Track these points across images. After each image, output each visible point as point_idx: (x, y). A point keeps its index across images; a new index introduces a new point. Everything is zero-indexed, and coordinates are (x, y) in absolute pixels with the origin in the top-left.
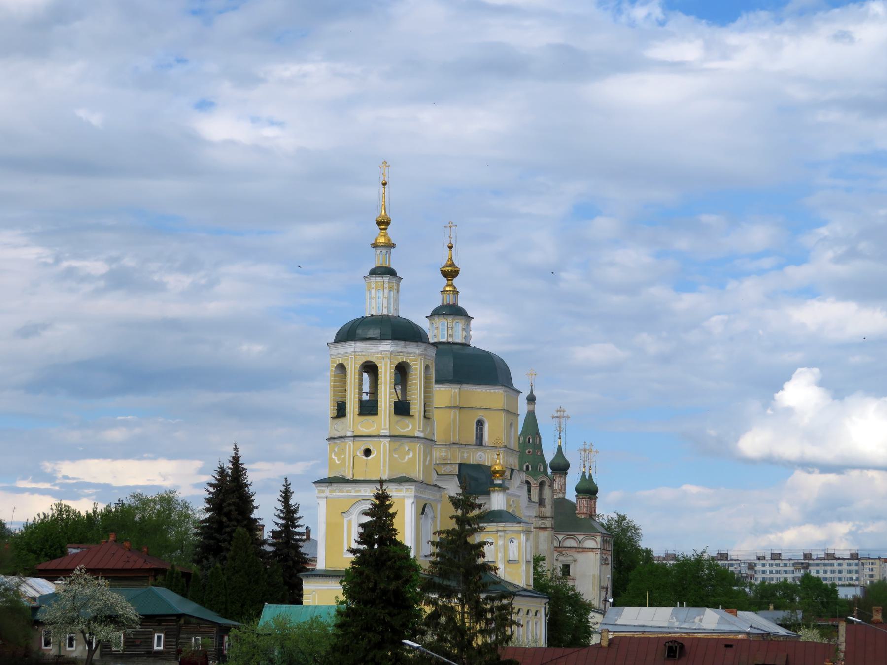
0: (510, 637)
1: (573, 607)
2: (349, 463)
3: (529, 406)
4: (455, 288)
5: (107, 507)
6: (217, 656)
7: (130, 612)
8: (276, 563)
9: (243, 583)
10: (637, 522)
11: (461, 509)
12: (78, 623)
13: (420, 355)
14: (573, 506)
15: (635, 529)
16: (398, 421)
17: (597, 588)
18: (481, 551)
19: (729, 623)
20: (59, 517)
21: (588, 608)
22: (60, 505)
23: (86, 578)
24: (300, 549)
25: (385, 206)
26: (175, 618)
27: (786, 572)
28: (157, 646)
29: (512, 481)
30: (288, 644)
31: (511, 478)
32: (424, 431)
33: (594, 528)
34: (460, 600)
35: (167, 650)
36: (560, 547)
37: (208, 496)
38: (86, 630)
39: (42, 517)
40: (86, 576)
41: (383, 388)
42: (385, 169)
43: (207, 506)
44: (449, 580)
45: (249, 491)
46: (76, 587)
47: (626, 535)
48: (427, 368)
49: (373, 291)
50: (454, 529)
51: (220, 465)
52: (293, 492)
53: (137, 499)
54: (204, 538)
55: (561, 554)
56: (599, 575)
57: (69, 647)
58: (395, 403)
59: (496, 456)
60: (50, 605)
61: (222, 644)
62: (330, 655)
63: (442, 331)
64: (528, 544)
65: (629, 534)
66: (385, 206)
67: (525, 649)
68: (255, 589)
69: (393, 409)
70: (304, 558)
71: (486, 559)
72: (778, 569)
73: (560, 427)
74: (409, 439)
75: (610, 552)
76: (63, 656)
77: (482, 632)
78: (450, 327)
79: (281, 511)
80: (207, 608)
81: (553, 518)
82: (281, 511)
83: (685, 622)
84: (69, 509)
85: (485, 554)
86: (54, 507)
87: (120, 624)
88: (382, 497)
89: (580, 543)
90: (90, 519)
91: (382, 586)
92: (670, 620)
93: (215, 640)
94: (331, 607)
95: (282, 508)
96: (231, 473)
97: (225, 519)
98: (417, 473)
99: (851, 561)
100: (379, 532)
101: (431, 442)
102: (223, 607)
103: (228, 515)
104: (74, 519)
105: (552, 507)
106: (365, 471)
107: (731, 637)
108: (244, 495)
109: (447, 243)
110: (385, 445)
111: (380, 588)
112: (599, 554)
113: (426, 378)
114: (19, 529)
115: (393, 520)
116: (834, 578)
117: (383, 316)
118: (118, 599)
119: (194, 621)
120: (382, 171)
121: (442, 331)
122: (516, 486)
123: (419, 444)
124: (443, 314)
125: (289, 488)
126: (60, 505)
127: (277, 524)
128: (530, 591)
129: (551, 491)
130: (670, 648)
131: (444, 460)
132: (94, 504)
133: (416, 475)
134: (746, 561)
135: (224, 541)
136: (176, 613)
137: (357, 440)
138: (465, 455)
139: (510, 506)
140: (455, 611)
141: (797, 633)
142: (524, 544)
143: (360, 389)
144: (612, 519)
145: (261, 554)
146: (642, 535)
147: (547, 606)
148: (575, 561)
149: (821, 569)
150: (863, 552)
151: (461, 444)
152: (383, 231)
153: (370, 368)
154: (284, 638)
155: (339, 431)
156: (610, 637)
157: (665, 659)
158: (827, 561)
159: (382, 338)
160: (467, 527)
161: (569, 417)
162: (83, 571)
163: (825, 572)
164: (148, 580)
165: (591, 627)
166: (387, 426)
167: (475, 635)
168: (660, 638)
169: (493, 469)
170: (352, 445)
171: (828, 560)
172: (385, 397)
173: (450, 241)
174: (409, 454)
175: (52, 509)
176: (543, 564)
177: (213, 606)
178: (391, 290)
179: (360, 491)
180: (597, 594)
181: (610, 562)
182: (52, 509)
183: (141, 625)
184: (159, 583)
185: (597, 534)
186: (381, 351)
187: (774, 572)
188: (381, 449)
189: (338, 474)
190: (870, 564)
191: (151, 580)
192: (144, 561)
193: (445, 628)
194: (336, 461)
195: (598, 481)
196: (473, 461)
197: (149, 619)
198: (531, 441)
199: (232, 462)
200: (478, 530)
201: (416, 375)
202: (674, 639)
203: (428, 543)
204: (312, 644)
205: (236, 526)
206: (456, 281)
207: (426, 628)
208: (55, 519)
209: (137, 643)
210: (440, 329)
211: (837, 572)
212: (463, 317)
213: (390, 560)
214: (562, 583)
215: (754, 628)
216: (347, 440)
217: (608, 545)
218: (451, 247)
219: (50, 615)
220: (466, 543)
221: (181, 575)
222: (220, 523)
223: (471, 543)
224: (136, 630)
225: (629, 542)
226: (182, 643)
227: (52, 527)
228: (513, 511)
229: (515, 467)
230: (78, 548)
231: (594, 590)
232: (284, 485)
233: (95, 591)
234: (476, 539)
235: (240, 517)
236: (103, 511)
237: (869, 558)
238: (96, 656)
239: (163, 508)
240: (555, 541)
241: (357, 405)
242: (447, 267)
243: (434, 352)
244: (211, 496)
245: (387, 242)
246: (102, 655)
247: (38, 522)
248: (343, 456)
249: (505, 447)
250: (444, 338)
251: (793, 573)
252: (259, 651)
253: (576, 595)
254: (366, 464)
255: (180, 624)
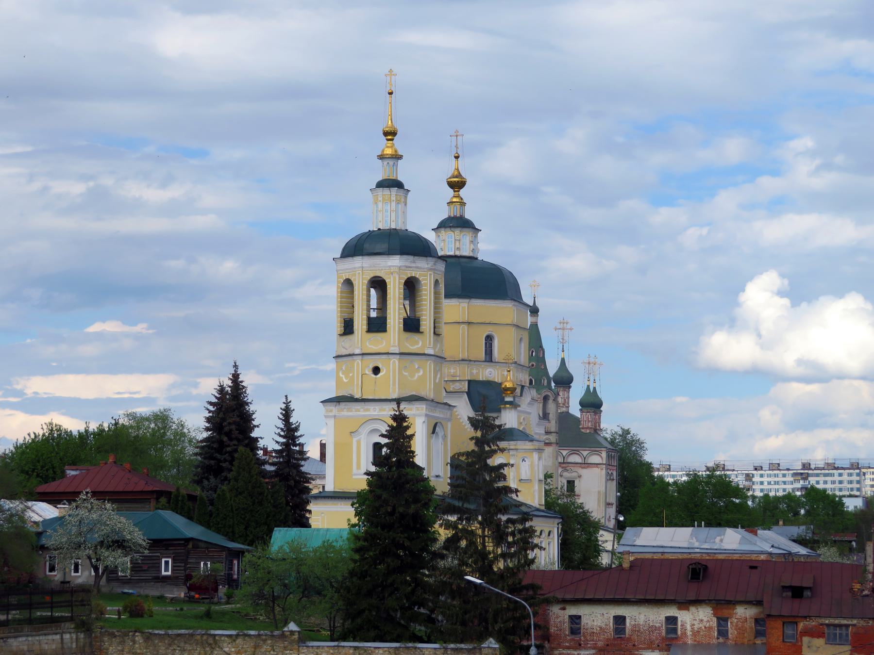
0: (533, 561)
1: (581, 525)
2: (357, 381)
3: (532, 318)
4: (462, 199)
5: (99, 426)
6: (226, 581)
7: (138, 537)
8: (278, 482)
9: (246, 504)
10: (641, 437)
11: (480, 430)
12: (85, 549)
13: (430, 269)
14: (577, 421)
15: (640, 444)
16: (407, 338)
17: (603, 505)
18: (502, 473)
19: (750, 543)
20: (50, 436)
21: (596, 526)
22: (51, 424)
23: (92, 503)
24: (301, 468)
25: (391, 117)
26: (183, 542)
27: (785, 483)
28: (165, 572)
29: (523, 398)
30: (304, 569)
31: (521, 395)
32: (434, 348)
33: (599, 443)
34: (480, 523)
35: (175, 575)
36: (564, 463)
37: (208, 415)
38: (93, 556)
39: (33, 436)
40: (92, 500)
41: (392, 304)
42: (391, 78)
43: (207, 425)
44: (469, 502)
45: (249, 409)
46: (83, 512)
47: (630, 450)
48: (437, 282)
49: (380, 204)
50: (473, 451)
51: (220, 383)
52: (294, 410)
53: (131, 418)
54: (205, 458)
55: (565, 470)
56: (604, 491)
57: (74, 572)
58: (404, 319)
59: (506, 373)
60: (55, 530)
61: (231, 569)
62: (347, 580)
63: (449, 244)
64: (541, 462)
65: (634, 448)
66: (391, 117)
67: (544, 571)
68: (259, 511)
69: (402, 326)
70: (306, 478)
71: (506, 484)
72: (776, 479)
73: (563, 339)
74: (420, 356)
75: (616, 467)
76: (69, 582)
77: (504, 556)
78: (457, 240)
79: (282, 429)
80: (214, 531)
81: (557, 433)
82: (282, 429)
83: (706, 542)
84: (60, 428)
85: (506, 476)
86: (45, 427)
87: (128, 549)
88: (400, 418)
89: (585, 459)
90: (84, 437)
91: (401, 510)
92: (690, 541)
93: (224, 564)
94: (344, 530)
95: (282, 426)
96: (231, 390)
97: (225, 439)
98: (427, 391)
99: (851, 471)
100: (396, 455)
101: (441, 359)
102: (231, 530)
103: (229, 434)
104: (66, 438)
105: (556, 422)
106: (375, 390)
107: (754, 557)
108: (245, 414)
109: (454, 153)
110: (394, 362)
111: (399, 512)
112: (604, 470)
113: (435, 293)
114: (9, 449)
115: (411, 442)
116: (834, 488)
117: (390, 230)
118: (125, 524)
119: (203, 545)
120: (388, 81)
121: (449, 244)
122: (527, 403)
123: (429, 362)
124: (450, 227)
125: (290, 405)
126: (51, 424)
127: (277, 442)
128: (543, 511)
129: (555, 405)
130: (694, 570)
131: (453, 377)
132: (86, 423)
133: (427, 393)
134: (743, 472)
135: (225, 461)
136: (184, 537)
137: (366, 357)
138: (475, 371)
139: (521, 423)
140: (476, 535)
141: (816, 552)
142: (537, 463)
143: (368, 305)
144: (616, 433)
145: (263, 474)
146: (646, 449)
147: (560, 526)
148: (580, 477)
149: (821, 479)
150: (863, 461)
151: (470, 361)
152: (390, 142)
153: (379, 284)
154: (300, 563)
155: (346, 349)
156: (632, 559)
157: (689, 581)
158: (827, 472)
159: (390, 252)
160: (487, 448)
161: (573, 329)
162: (89, 495)
163: (825, 482)
164: (150, 502)
165: (601, 546)
166: (397, 344)
167: (496, 558)
168: (683, 560)
169: (503, 386)
170: (360, 363)
171: (829, 470)
172: (394, 311)
173: (457, 150)
174: (419, 372)
175: (42, 428)
176: (551, 482)
177: (219, 529)
178: (398, 203)
179: (368, 410)
180: (603, 510)
181: (615, 478)
182: (42, 428)
183: (148, 550)
184: (162, 506)
185: (602, 449)
186: (390, 267)
187: (772, 483)
188: (391, 367)
189: (347, 393)
190: (870, 474)
191: (153, 503)
192: (145, 483)
193: (465, 553)
194: (344, 379)
195: (602, 395)
196: (482, 378)
197: (159, 545)
198: (534, 354)
199: (231, 379)
200: (499, 451)
201: (426, 290)
202: (697, 561)
203: (447, 465)
204: (329, 570)
205: (238, 445)
206: (463, 192)
207: (445, 552)
208: (45, 439)
209: (144, 568)
210: (447, 241)
211: (837, 482)
212: (471, 229)
213: (408, 483)
214: (570, 501)
215: (776, 548)
216: (355, 357)
217: (613, 460)
218: (457, 157)
219: (56, 541)
220: (486, 465)
221: (186, 497)
222: (221, 443)
223: (491, 465)
224: (143, 555)
225: (634, 456)
226: (190, 567)
227: (43, 447)
228: (524, 428)
229: (525, 383)
230: (76, 470)
231: (600, 506)
232: (284, 403)
233: (101, 515)
234: (496, 460)
235: (241, 437)
236: (96, 430)
237: (869, 468)
238: (103, 581)
239: (158, 427)
240: (559, 457)
241: (365, 322)
242: (454, 178)
243: (443, 267)
244: (211, 415)
245: (394, 153)
246: (109, 580)
247: (28, 442)
248: (351, 375)
249: (516, 363)
250: (451, 251)
251: (793, 484)
252: (274, 576)
253: (585, 513)
254: (375, 382)
255: (188, 548)
